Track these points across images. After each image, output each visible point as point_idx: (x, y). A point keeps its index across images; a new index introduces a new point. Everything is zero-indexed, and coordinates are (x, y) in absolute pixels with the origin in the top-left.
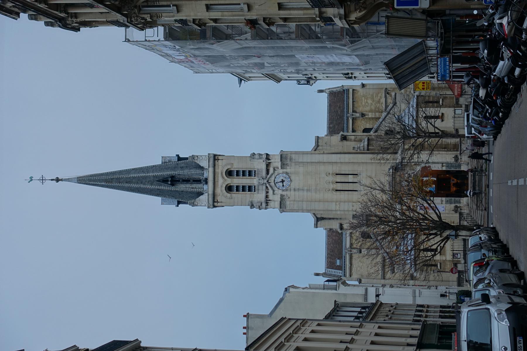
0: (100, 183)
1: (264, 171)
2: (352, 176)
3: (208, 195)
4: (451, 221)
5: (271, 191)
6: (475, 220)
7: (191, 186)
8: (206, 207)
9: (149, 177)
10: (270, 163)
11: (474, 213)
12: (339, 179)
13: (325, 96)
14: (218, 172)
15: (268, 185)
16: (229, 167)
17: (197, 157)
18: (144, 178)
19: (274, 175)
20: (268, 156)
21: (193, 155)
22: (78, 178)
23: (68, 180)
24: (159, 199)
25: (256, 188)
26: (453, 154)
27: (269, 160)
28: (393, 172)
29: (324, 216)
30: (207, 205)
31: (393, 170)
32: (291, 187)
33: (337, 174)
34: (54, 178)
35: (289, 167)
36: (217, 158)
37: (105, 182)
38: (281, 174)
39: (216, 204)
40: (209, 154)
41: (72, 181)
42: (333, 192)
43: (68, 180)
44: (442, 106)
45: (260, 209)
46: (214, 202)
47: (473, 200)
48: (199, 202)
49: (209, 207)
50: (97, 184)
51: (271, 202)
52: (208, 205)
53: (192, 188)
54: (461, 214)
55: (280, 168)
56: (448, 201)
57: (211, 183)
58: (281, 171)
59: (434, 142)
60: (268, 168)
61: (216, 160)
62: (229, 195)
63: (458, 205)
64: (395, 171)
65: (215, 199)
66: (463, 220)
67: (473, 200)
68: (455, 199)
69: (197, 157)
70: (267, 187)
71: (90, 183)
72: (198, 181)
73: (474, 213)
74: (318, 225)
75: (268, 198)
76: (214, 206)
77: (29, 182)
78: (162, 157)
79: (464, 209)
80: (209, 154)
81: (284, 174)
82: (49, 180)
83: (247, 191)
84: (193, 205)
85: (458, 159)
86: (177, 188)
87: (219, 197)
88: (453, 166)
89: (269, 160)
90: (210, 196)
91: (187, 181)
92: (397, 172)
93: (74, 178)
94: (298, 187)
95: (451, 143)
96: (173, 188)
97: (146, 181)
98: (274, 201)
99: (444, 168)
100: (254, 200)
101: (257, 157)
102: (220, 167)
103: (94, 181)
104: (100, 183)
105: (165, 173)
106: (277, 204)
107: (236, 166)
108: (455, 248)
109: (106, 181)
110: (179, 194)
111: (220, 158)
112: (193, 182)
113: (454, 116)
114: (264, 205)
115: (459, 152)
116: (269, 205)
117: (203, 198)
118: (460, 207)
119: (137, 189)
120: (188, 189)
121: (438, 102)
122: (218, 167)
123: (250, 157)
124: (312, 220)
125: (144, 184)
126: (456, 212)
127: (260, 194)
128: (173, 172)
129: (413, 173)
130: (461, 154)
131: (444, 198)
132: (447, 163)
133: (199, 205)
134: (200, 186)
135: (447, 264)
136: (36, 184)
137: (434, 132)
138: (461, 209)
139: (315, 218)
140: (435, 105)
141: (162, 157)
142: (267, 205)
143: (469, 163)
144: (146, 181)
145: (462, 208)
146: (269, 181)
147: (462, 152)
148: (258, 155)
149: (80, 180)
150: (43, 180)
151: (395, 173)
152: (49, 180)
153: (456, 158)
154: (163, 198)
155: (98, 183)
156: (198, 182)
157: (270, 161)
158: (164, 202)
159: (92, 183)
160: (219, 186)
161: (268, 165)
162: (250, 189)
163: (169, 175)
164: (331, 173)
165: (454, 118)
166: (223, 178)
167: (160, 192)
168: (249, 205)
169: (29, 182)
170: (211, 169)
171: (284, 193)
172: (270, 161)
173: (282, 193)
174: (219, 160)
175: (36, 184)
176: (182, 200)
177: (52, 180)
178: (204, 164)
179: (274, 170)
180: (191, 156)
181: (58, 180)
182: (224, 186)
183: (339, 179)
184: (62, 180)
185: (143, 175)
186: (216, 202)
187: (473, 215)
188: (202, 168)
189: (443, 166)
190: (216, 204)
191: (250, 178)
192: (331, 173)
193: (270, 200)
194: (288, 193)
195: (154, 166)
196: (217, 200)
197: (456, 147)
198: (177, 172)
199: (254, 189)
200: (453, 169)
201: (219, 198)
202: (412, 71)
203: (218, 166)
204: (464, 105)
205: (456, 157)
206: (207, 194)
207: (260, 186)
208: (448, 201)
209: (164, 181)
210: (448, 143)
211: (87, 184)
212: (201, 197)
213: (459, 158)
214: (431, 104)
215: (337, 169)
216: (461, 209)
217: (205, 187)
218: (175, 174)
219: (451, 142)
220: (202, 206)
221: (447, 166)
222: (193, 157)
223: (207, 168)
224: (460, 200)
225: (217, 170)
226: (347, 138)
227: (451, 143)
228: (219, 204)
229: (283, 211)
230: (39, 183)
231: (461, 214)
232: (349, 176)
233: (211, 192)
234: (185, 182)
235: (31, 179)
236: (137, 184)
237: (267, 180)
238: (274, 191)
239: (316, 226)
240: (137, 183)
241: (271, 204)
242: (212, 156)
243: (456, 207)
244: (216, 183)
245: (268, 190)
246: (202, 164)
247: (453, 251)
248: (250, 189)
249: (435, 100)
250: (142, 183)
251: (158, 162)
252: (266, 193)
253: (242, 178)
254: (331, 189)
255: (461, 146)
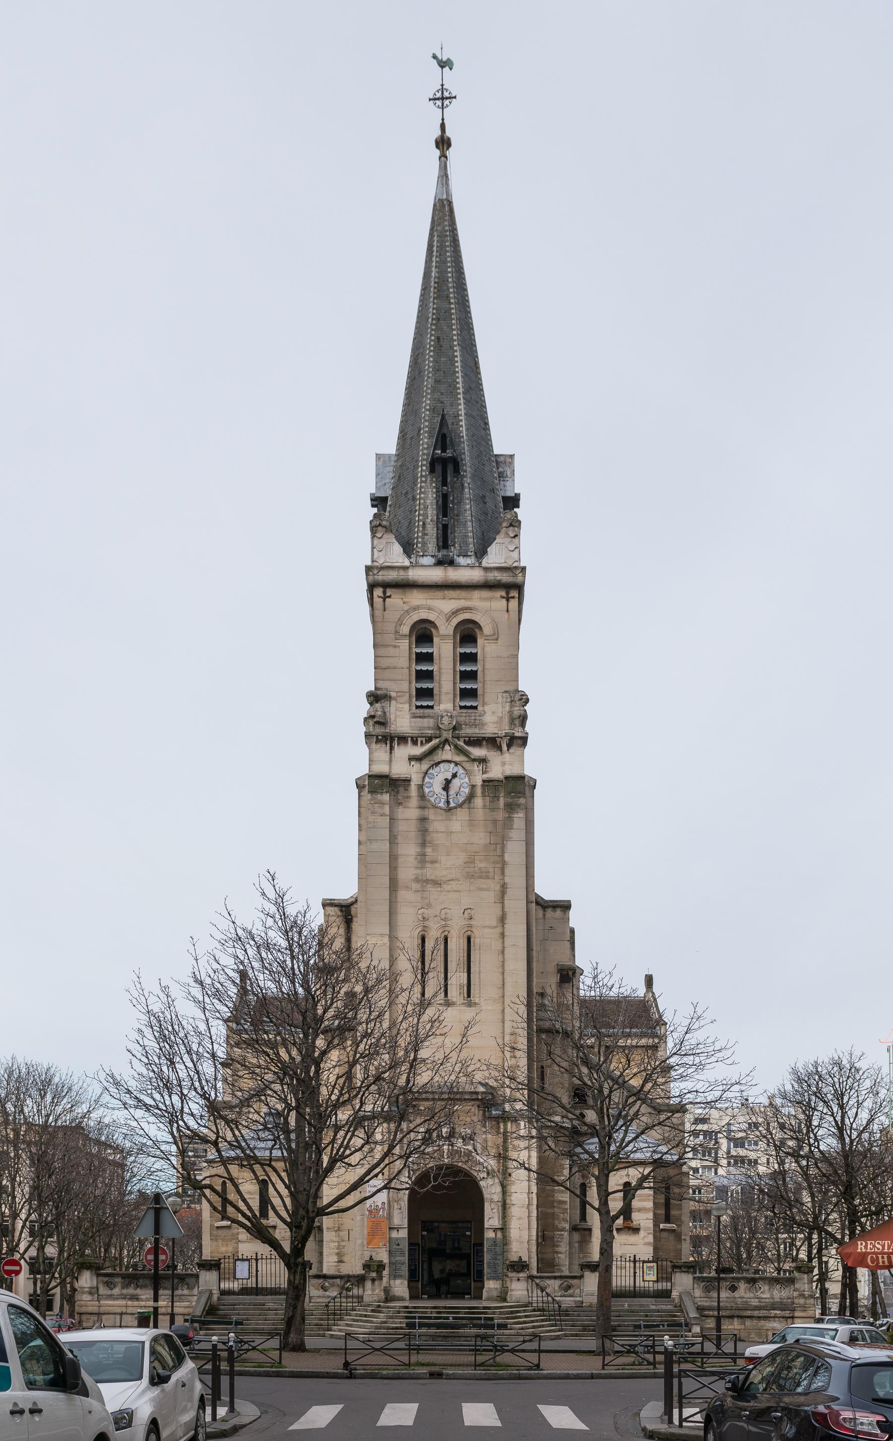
0: (434, 264)
1: (477, 731)
2: (466, 982)
3: (405, 568)
4: (344, 1255)
5: (418, 750)
6: (341, 1320)
7: (429, 520)
8: (369, 563)
9: (455, 403)
10: (499, 748)
11: (361, 1315)
12: (456, 946)
13: (641, 992)
14: (470, 599)
15: (435, 742)
16: (487, 630)
17: (516, 536)
18: (453, 386)
19: (466, 759)
20: (519, 742)
21: (520, 522)
22: (450, 203)
23: (444, 176)
24: (390, 447)
25: (427, 711)
26: (529, 1257)
27: (509, 746)
28: (477, 1093)
29: (355, 926)
30: (375, 564)
31: (483, 1093)
32: (432, 811)
33: (469, 939)
34: (448, 133)
35: (487, 804)
36: (511, 595)
37: (438, 278)
38: (467, 780)
39: (378, 592)
40: (524, 569)
41: (440, 185)
42: (420, 929)
43: (444, 176)
44: (657, 1229)
45: (365, 719)
46: (386, 585)
47: (399, 1312)
48: (383, 541)
49: (368, 569)
50: (431, 258)
51: (386, 752)
52: (377, 567)
53: (424, 524)
54: (360, 1280)
55: (485, 776)
56: (398, 1245)
57: (437, 574)
58: (478, 780)
59: (559, 1208)
60: (484, 743)
61: (508, 593)
62: (406, 629)
63: (385, 1273)
64: (482, 1099)
65: (393, 590)
66: (343, 1288)
67: (399, 1312)
68: (403, 1264)
69: (516, 536)
70: (429, 739)
71: (435, 238)
72: (444, 542)
73: (361, 1315)
74: (329, 909)
75: (398, 745)
76: (371, 587)
77: (435, 57)
78: (512, 456)
79: (373, 1290)
80: (524, 569)
81: (467, 791)
82: (443, 119)
83: (419, 686)
84: (375, 527)
85: (518, 1272)
86: (425, 482)
87: (400, 602)
88: (496, 1259)
89: (509, 746)
90: (402, 573)
91: (444, 506)
92: (479, 1107)
93: (448, 193)
94: (431, 829)
95: (558, 1253)
96: (423, 469)
97: (442, 394)
98: (391, 761)
99: (489, 1235)
100: (393, 703)
101: (517, 711)
102: (487, 604)
103: (441, 248)
104: (434, 264)
105: (466, 448)
106: (383, 769)
107: (484, 648)
108: (264, 1266)
109: (441, 282)
110: (407, 493)
111: (514, 603)
112: (440, 526)
113: (637, 1259)
114: (379, 730)
115: (535, 1273)
116: (379, 746)
117: (395, 555)
118: (380, 1278)
119: (420, 372)
120: (421, 512)
121: (668, 1220)
122: (486, 599)
123: (517, 691)
124: (346, 890)
125: (434, 390)
126: (367, 1266)
127: (410, 722)
128: (469, 469)
129: (476, 1150)
130: (531, 1277)
131: (406, 1236)
132: (505, 1241)
133: (376, 541)
134: (432, 547)
135: (227, 1245)
136: (432, 78)
137: (610, 1190)
138: (373, 1280)
139: (350, 901)
140: (659, 1212)
141: (512, 456)
142: (378, 741)
143: (505, 1300)
144: (442, 394)
145: (376, 1283)
146: (447, 747)
147: (538, 1281)
148: (522, 712)
149: (443, 206)
150: (443, 98)
151: (473, 1100)
152: (443, 119)
153: (520, 1266)
154: (393, 459)
155: (434, 259)
156: (441, 539)
157: (505, 748)
158: (384, 462)
159: (435, 243)
160: (430, 603)
161: (493, 742)
162: (425, 694)
163: (462, 460)
164: (472, 922)
165: (632, 1259)
166: (455, 613)
167: (412, 438)
168: (376, 688)
169: (435, 57)
170: (476, 575)
171: (413, 790)
172: (505, 748)
173: (412, 783)
174: (508, 600)
175: (432, 78)
176: (390, 506)
177: (443, 126)
178: (496, 556)
179: (483, 761)
180: (517, 516)
181: (443, 143)
182: (432, 617)
183: (456, 946)
184: (443, 156)
185: (460, 385)
186: (384, 593)
187: (356, 1315)
188: (481, 553)
189: (495, 1230)
190: (378, 592)
191: (455, 695)
192: (472, 922)
193: (392, 748)
194: (414, 801)
195: (487, 424)
196: (389, 597)
197: (547, 1265)
198: (469, 481)
199: (425, 704)
200: (487, 1258)
201: (396, 600)
202: (512, 1312)
203: (490, 599)
204: (669, 1288)
205: (523, 1266)
206: (407, 563)
207: (431, 720)
208: (398, 1245)
209: (443, 439)
210: (558, 1246)
211: (432, 229)
212: (397, 549)
213: (521, 1275)
214: (662, 1200)
215: (485, 938)
216: (373, 1280)
217: (428, 560)
218: (464, 476)
219: (560, 1253)
220: (372, 551)
221: (494, 1241)
222: (515, 523)
223: (484, 564)
224: (401, 1277)
225: (477, 594)
226: (567, 985)
227: (558, 1253)
228: (378, 601)
229: (360, 787)
230: (433, 89)
231: (360, 1280)
232: (466, 974)
233: (416, 575)
234: (440, 502)
235: (444, 64)
236: (434, 368)
237: (450, 739)
238: (419, 759)
239: (326, 904)
240: (436, 370)
241: (382, 752)
242: (519, 579)
243: (380, 1267)
244: (439, 593)
245: (422, 742)
246: (493, 549)
247: (257, 1260)
248: (425, 694)
249: (673, 1212)
250: (437, 381)
251: (499, 448)
252: (412, 738)
253: (454, 671)
254: (426, 923)
255: (555, 1278)
